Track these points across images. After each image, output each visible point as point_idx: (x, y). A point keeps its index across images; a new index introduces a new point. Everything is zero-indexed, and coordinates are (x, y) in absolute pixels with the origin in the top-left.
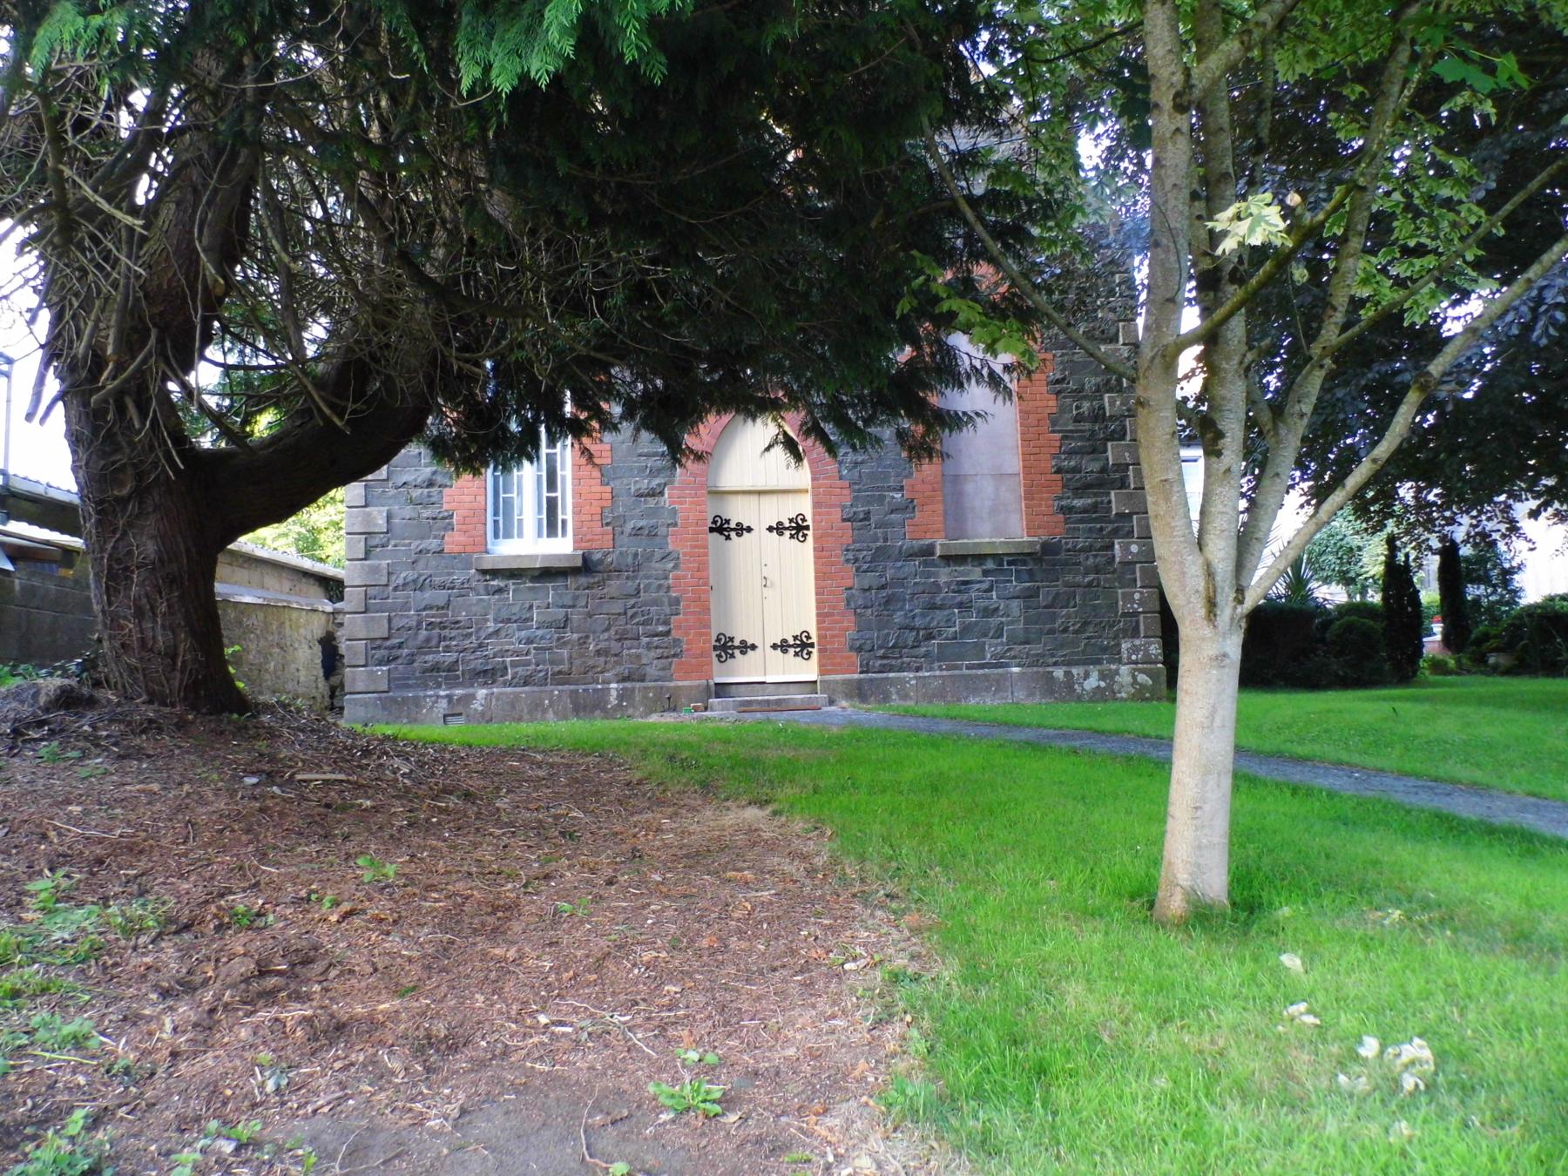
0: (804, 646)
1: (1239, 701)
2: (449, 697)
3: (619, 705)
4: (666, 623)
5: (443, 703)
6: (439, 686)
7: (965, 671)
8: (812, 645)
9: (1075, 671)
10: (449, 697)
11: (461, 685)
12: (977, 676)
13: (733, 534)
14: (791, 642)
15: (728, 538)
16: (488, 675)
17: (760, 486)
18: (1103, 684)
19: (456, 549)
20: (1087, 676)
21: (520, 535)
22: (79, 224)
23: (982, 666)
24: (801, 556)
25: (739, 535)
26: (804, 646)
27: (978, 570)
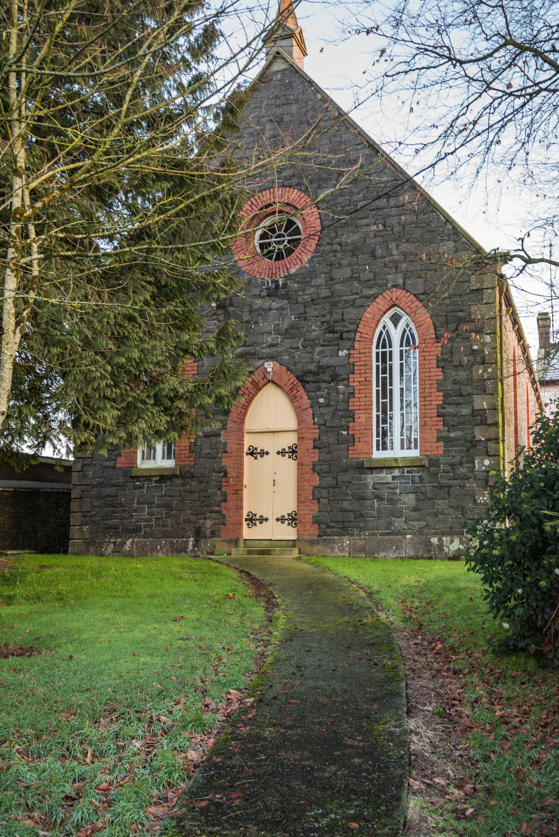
0: (251, 520)
1: (93, 546)
2: (114, 543)
3: (193, 550)
4: (219, 506)
5: (112, 546)
6: (111, 537)
7: (379, 537)
8: (246, 520)
9: (444, 539)
10: (114, 543)
11: (120, 537)
12: (385, 540)
13: (258, 456)
14: (286, 517)
15: (256, 458)
16: (136, 530)
17: (272, 428)
18: (462, 547)
19: (121, 466)
20: (452, 542)
21: (154, 458)
22: (149, 226)
23: (389, 534)
24: (288, 468)
25: (262, 456)
26: (251, 520)
27: (390, 476)
